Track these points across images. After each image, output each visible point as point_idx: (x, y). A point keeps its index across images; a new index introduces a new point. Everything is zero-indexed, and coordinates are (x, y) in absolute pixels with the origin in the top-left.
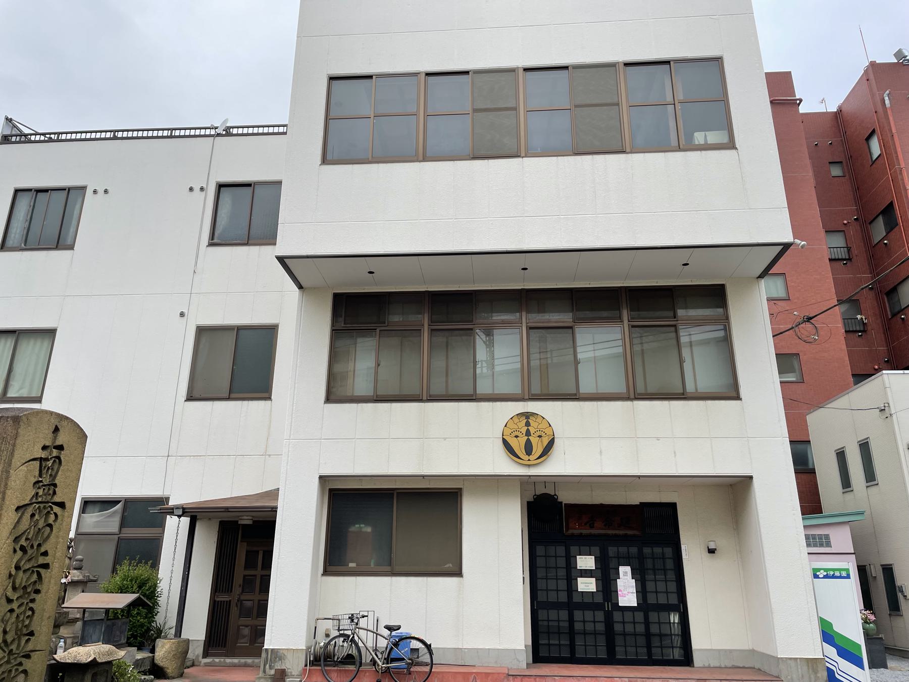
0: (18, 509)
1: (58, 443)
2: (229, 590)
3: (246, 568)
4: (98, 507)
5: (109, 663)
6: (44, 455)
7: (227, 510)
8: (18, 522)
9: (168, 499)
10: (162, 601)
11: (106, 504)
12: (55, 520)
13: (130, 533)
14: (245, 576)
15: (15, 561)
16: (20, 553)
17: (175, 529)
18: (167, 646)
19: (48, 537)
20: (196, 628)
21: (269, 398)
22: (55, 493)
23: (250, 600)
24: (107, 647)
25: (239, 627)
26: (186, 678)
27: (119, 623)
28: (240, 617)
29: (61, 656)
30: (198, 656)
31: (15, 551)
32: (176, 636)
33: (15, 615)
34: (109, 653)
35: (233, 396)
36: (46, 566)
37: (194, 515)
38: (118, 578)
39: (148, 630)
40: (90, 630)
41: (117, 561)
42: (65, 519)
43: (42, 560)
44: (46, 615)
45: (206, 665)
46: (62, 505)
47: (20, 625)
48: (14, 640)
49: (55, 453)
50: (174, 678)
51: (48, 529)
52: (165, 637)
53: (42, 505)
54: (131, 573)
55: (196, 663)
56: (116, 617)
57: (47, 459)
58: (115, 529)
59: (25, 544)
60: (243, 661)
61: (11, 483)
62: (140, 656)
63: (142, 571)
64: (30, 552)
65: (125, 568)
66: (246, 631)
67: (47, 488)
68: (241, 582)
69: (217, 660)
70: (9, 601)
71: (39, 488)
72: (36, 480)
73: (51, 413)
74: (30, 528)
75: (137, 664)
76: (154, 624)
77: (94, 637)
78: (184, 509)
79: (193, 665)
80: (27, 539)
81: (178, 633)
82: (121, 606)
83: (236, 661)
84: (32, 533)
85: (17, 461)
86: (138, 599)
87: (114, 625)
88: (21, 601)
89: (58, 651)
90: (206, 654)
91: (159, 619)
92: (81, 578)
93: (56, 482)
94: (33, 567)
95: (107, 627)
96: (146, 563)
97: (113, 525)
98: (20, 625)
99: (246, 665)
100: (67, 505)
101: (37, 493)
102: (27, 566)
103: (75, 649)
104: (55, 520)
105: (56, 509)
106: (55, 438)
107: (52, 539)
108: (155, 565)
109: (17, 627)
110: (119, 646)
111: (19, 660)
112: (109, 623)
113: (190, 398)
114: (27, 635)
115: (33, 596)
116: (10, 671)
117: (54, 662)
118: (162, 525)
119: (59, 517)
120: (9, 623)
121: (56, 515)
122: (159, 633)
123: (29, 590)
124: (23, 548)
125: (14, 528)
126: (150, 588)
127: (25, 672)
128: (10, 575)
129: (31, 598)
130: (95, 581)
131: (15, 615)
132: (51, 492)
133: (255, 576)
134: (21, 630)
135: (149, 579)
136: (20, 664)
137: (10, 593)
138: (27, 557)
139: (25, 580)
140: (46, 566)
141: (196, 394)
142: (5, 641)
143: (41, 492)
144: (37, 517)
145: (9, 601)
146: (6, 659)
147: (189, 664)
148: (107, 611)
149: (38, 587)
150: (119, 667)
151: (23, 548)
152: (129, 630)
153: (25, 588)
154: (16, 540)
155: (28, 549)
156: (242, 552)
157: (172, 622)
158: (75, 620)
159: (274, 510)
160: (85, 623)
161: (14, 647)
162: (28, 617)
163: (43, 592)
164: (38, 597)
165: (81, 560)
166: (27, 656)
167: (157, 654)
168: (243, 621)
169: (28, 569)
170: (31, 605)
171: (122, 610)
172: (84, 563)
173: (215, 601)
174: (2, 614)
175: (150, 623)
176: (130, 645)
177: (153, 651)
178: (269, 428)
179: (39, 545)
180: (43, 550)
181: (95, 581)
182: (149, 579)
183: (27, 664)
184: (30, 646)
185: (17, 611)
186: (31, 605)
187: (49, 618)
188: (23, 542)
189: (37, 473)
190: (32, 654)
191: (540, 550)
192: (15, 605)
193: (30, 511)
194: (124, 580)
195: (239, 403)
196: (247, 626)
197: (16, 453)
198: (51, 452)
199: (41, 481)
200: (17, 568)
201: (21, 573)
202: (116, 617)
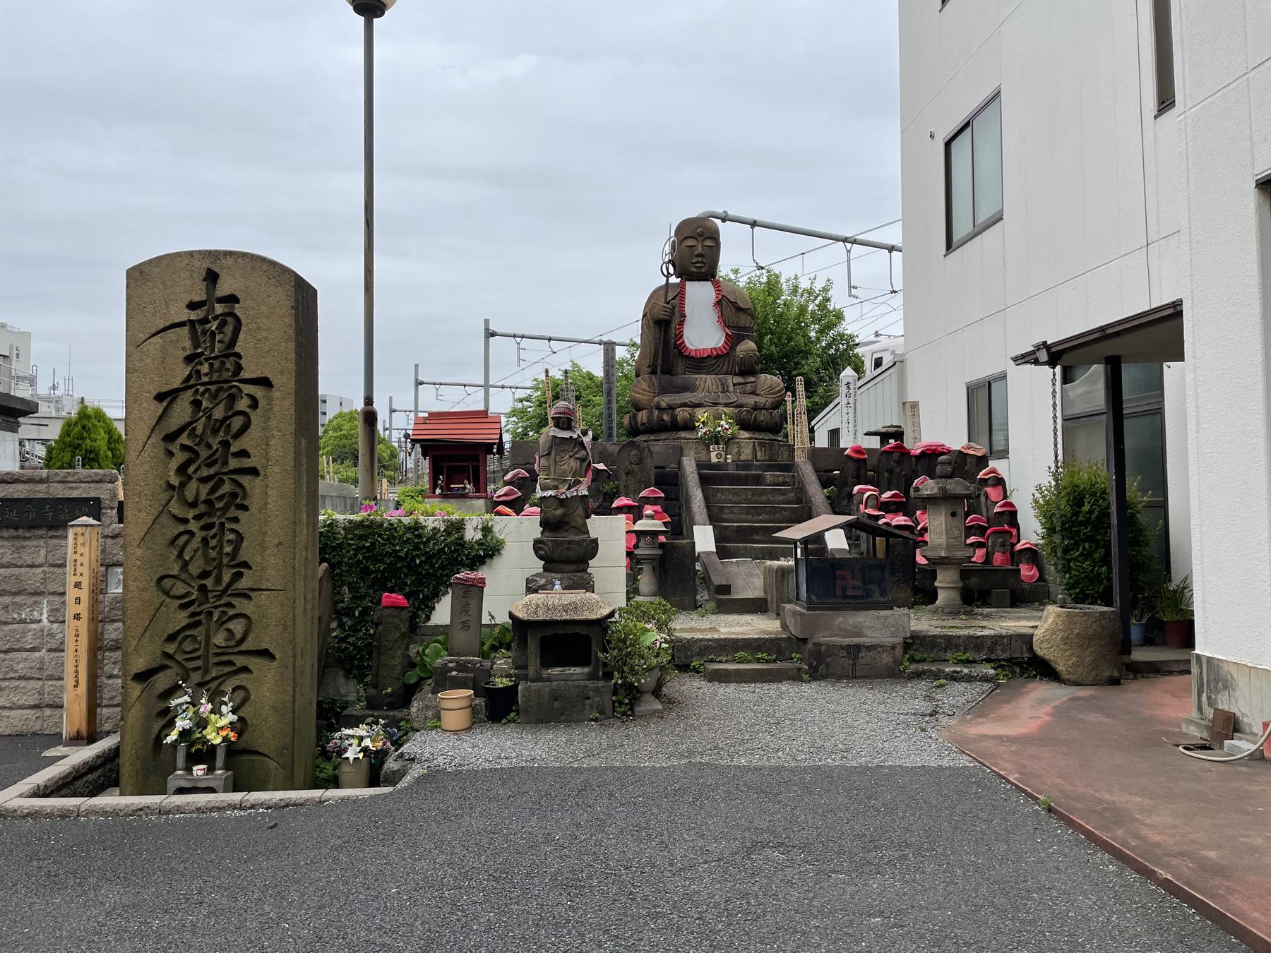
6: (194, 316)
36: (254, 472)
53: (213, 388)
72: (188, 352)
102: (205, 472)
107: (253, 432)
190: (252, 594)
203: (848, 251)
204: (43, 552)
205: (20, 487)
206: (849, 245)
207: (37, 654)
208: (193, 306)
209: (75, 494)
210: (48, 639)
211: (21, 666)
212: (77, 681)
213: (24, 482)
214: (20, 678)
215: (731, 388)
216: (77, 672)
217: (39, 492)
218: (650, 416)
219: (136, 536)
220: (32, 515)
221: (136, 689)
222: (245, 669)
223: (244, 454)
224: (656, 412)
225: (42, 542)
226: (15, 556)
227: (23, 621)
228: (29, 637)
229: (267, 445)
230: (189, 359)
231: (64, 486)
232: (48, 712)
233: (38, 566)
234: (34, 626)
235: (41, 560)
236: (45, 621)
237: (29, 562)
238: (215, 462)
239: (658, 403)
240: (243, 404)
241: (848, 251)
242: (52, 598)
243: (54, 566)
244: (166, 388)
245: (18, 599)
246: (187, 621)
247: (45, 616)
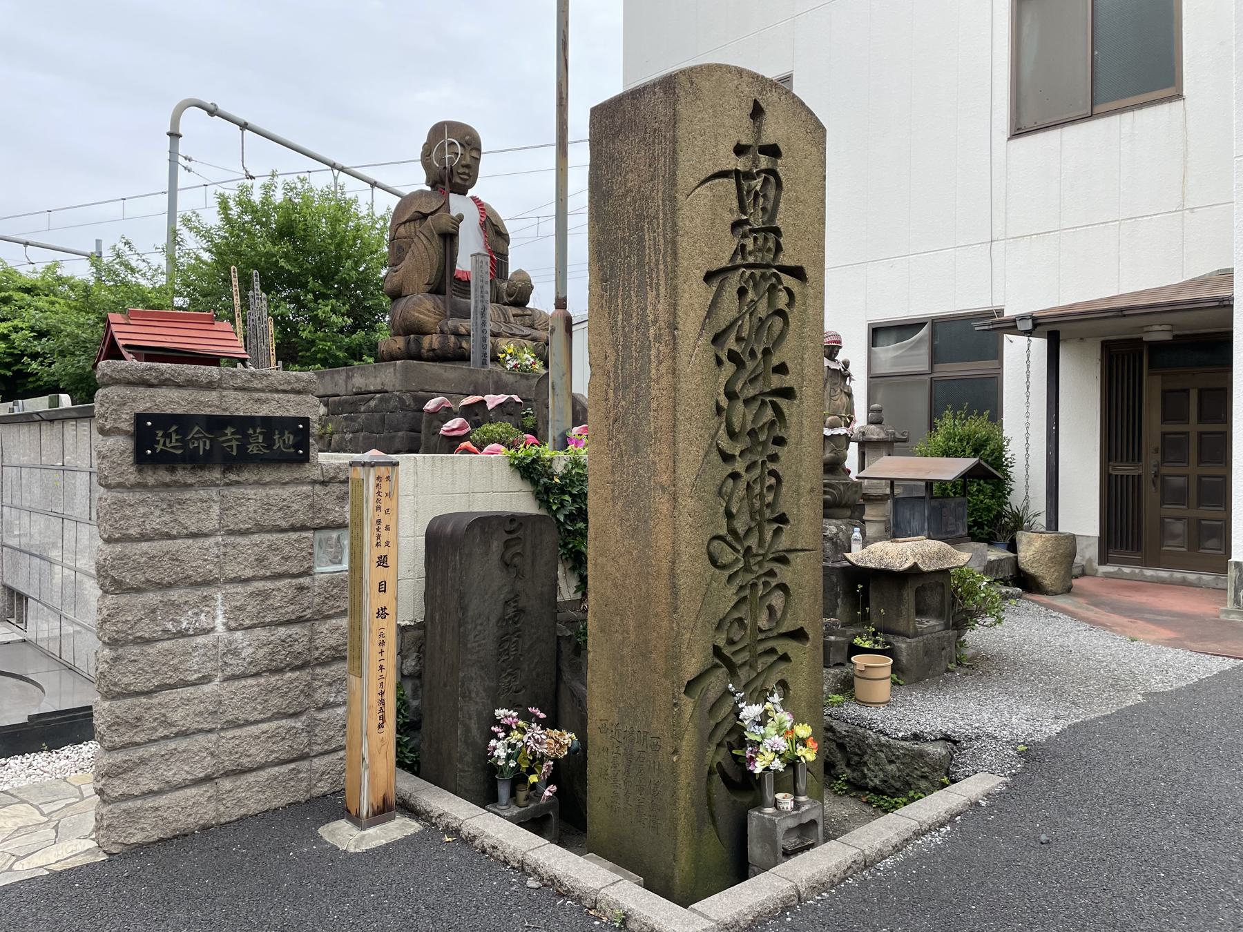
0: (709, 277)
1: (768, 139)
2: (1135, 455)
3: (1165, 419)
4: (894, 334)
5: (945, 572)
6: (741, 164)
7: (1120, 313)
8: (714, 304)
9: (1000, 312)
10: (1016, 472)
11: (905, 329)
12: (791, 303)
13: (948, 370)
14: (1164, 434)
15: (723, 380)
16: (729, 368)
17: (1021, 359)
18: (1038, 544)
19: (782, 335)
20: (1082, 515)
21: (1179, 96)
22: (779, 248)
23: (1183, 474)
24: (936, 545)
25: (1162, 520)
26: (1077, 595)
27: (952, 503)
28: (1163, 503)
29: (858, 555)
30: (1090, 560)
31: (719, 362)
32: (1049, 527)
33: (742, 485)
34: (941, 556)
35: (1098, 109)
36: (788, 393)
37: (1054, 330)
38: (939, 438)
39: (999, 516)
40: (906, 513)
41: (934, 413)
42: (810, 302)
43: (776, 381)
44: (805, 486)
45: (1107, 576)
46: (798, 273)
47: (757, 504)
48: (750, 530)
49: (764, 162)
50: (1056, 594)
51: (778, 322)
52: (1029, 529)
53: (758, 272)
54: (959, 430)
55: (1088, 571)
56: (944, 495)
57: (748, 176)
58: (924, 366)
59: (735, 348)
60: (1178, 575)
61: (684, 224)
62: (994, 554)
63: (977, 426)
64: (750, 365)
65: (947, 422)
66: (1179, 527)
67: (761, 236)
68: (1157, 442)
69: (1127, 570)
70: (727, 458)
71: (744, 236)
72: (735, 217)
73: (740, 72)
74: (741, 317)
75: (990, 568)
76: (1007, 508)
77: (915, 524)
78: (1034, 319)
79: (1083, 574)
80: (739, 339)
81: (1053, 522)
82: (949, 476)
83: (1164, 574)
84: (747, 326)
85: (687, 177)
86: (978, 465)
87: (943, 506)
88: (750, 458)
89: (854, 546)
90: (1104, 560)
91: (1015, 500)
92: (882, 436)
93: (778, 223)
94: (762, 394)
95: (933, 509)
96: (980, 414)
97: (920, 361)
98: (757, 504)
99: (1184, 583)
100: (810, 273)
101: (743, 247)
102: (751, 392)
103: (878, 545)
104: (791, 303)
105: (788, 280)
106: (758, 131)
107: (791, 341)
108: (996, 416)
109: (752, 506)
110: (954, 541)
111: (768, 566)
112: (933, 503)
113: (1018, 132)
114: (776, 520)
115: (772, 449)
116: (754, 585)
117: (846, 564)
118: (997, 354)
119: (798, 297)
120: (735, 499)
121: (789, 292)
122: (1018, 522)
123: (762, 438)
124: (733, 357)
125: (708, 315)
126: (993, 451)
127: (783, 587)
128: (719, 410)
129: (770, 452)
130: (905, 441)
131: (742, 485)
132: (771, 244)
133: (1186, 433)
134: (760, 511)
135: (988, 439)
136: (771, 573)
137: (725, 443)
138: (745, 376)
139: (750, 418)
140: (788, 393)
141: (1027, 123)
142: (733, 531)
143: (749, 243)
144: (751, 295)
145: (727, 458)
146: (741, 565)
147: (1076, 571)
148: (929, 484)
149: (778, 432)
150: (962, 579)
151: (733, 357)
152: (970, 515)
153: (753, 433)
154: (717, 339)
155: (746, 357)
156: (1152, 388)
157: (1039, 503)
158: (881, 499)
159: (1226, 305)
160: (897, 502)
161: (752, 542)
162: (770, 488)
163: (791, 441)
164: (782, 452)
165: (879, 411)
166: (782, 560)
167: (1021, 555)
168: (1170, 510)
169: (754, 398)
170: (771, 466)
171: (954, 483)
172: (884, 415)
173: (1109, 475)
174: (718, 482)
175: (1000, 506)
176: (974, 538)
177: (1013, 547)
178: (1185, 156)
179: (767, 352)
180: (775, 361)
181: (905, 441)
182: (988, 439)
183: (785, 574)
184: (784, 542)
185: (746, 477)
186: (771, 466)
187: (812, 490)
188: (731, 343)
189: (735, 204)
190: (791, 556)
191: (923, 484)
192: (739, 466)
193: (734, 281)
194: (949, 440)
195: (1114, 119)
196: (1179, 519)
197: (681, 157)
198: (755, 161)
199: (746, 222)
200: (731, 395)
201: (740, 406)
202: (944, 495)
203: (336, 178)
204: (216, 509)
205: (174, 394)
206: (336, 172)
207: (207, 688)
208: (740, 150)
209: (263, 411)
210: (230, 659)
211: (181, 713)
212: (383, 718)
213: (179, 386)
214: (184, 734)
215: (512, 319)
216: (382, 702)
217: (206, 405)
218: (444, 343)
219: (688, 481)
220: (203, 446)
221: (688, 705)
222: (785, 658)
223: (782, 369)
224: (452, 339)
225: (213, 493)
226: (167, 518)
227: (182, 634)
228: (195, 661)
229: (802, 359)
230: (736, 225)
231: (246, 395)
232: (227, 784)
233: (206, 535)
234: (200, 640)
235: (213, 524)
236: (220, 628)
237: (193, 529)
238: (756, 378)
239: (456, 327)
240: (782, 300)
241: (336, 178)
242: (231, 589)
243: (232, 533)
244: (715, 266)
245: (174, 595)
246: (736, 598)
247: (220, 620)
